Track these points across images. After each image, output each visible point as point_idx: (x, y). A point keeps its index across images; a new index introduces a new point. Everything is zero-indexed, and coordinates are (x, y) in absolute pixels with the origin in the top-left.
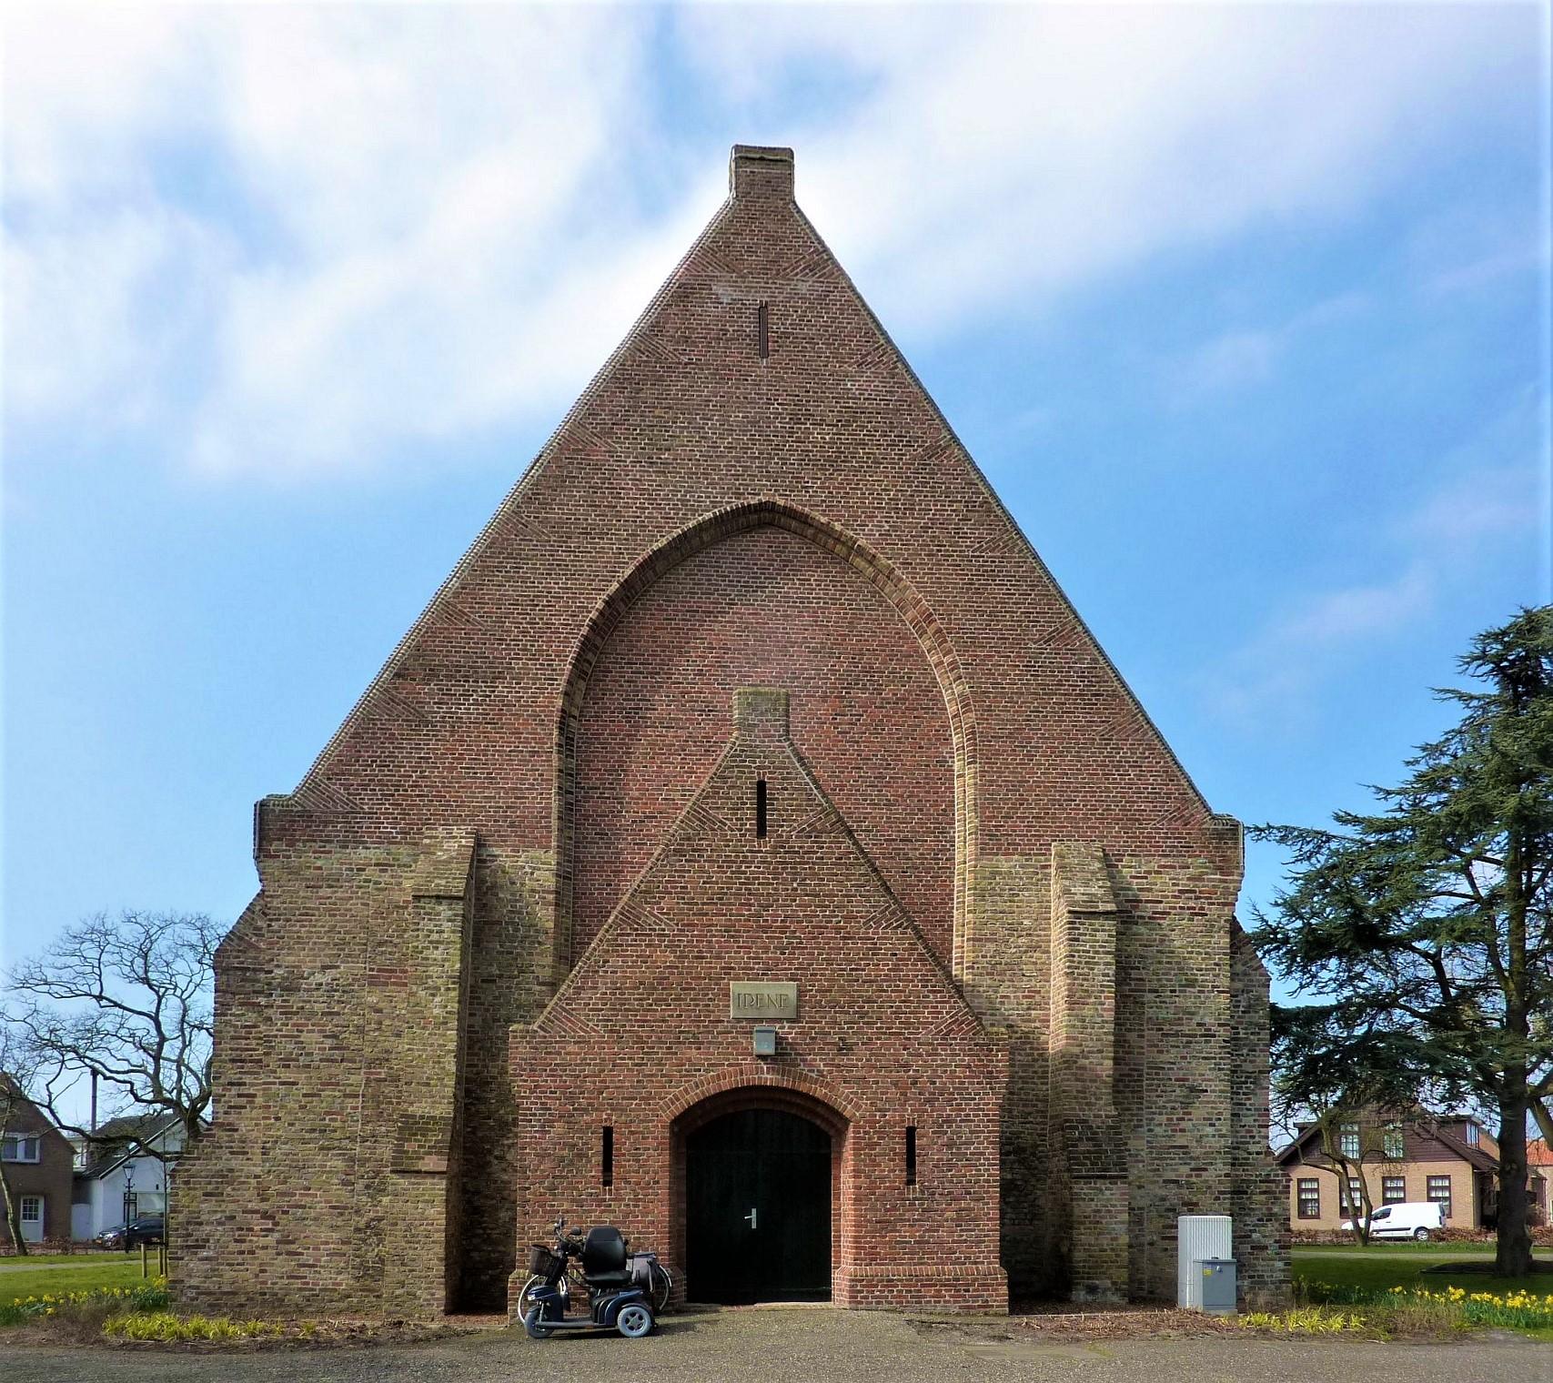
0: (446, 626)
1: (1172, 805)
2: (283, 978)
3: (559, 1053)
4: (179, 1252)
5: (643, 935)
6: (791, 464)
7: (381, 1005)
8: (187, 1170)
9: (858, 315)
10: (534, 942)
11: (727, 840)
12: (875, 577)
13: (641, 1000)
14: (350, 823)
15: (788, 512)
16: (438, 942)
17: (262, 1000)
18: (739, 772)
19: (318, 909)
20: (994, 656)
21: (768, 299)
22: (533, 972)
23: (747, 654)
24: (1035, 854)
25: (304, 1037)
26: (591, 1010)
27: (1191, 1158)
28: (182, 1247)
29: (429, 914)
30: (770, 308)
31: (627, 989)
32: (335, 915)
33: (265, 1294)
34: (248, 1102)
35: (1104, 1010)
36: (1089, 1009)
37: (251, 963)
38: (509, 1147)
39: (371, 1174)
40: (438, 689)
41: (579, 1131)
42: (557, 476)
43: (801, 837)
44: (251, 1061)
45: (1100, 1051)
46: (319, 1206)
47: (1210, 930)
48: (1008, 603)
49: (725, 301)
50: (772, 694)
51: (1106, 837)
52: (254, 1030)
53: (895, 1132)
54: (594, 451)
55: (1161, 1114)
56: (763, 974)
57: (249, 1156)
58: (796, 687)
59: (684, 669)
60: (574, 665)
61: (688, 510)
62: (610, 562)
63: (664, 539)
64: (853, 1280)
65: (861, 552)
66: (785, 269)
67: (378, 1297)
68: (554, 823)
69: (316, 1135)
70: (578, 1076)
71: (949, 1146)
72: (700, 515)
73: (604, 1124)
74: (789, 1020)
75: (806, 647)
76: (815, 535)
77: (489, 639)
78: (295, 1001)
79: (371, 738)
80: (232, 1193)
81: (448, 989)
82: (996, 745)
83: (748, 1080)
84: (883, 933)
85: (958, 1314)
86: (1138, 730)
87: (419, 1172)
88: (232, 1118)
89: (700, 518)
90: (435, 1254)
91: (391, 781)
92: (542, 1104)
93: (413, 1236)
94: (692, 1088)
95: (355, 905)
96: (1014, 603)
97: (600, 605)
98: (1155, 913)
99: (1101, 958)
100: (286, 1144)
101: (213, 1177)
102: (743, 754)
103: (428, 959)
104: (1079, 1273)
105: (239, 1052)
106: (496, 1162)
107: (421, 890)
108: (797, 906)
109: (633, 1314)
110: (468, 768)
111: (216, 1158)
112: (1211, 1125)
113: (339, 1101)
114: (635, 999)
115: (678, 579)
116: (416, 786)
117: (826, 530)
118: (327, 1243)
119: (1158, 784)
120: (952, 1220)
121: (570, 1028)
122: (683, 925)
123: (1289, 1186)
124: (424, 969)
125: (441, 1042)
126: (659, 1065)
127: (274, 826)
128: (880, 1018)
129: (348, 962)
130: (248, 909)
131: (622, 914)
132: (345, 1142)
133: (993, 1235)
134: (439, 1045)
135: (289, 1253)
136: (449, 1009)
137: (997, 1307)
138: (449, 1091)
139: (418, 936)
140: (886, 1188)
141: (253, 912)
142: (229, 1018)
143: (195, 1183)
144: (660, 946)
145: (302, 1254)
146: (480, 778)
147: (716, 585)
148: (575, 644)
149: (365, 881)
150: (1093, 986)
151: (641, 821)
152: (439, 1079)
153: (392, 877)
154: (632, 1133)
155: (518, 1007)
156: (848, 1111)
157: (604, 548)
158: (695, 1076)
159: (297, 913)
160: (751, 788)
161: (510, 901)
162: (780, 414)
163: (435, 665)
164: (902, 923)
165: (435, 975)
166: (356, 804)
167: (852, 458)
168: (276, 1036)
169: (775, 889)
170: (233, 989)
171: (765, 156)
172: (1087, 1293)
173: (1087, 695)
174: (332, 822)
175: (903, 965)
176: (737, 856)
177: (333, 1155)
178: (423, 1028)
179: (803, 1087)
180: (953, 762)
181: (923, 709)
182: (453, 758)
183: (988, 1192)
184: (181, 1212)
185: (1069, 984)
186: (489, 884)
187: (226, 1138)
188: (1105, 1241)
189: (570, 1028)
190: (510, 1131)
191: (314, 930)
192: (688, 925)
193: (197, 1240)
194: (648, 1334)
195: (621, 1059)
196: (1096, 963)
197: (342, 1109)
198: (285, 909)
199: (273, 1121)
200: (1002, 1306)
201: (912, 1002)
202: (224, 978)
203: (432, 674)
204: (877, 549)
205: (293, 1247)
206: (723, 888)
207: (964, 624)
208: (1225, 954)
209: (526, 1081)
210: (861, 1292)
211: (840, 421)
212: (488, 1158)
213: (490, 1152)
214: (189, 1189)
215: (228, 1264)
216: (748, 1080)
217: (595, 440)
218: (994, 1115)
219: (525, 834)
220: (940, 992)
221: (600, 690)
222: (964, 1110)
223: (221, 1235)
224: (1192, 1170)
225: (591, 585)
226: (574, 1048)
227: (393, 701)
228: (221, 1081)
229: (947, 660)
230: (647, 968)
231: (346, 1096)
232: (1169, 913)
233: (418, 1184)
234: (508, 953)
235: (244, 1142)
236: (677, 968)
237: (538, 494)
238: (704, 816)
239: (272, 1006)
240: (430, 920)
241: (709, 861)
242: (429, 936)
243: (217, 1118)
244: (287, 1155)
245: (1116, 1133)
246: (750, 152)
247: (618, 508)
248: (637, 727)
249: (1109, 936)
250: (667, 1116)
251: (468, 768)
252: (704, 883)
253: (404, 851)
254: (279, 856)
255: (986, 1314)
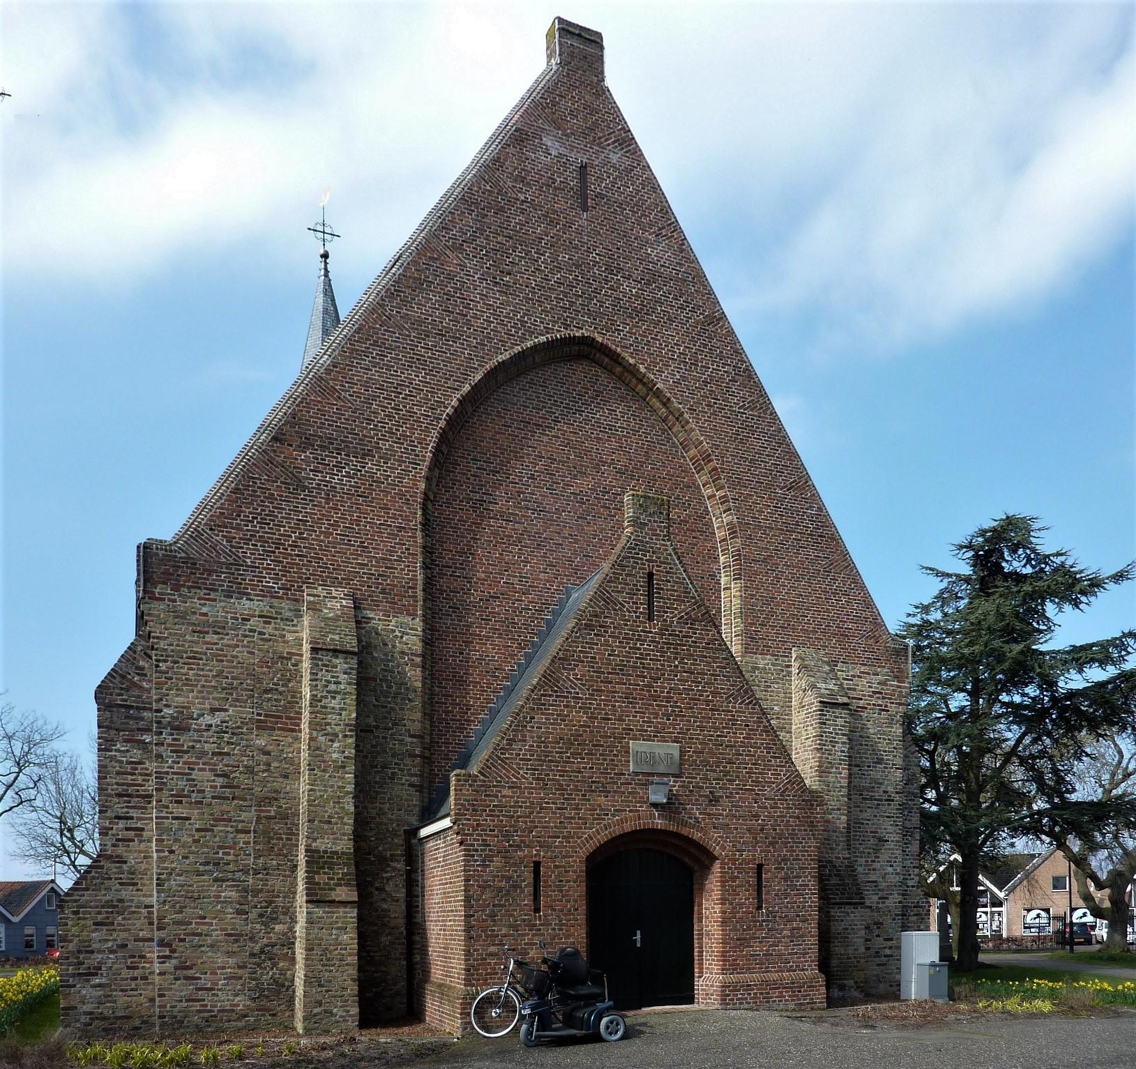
0: (319, 399)
1: (868, 627)
2: (172, 717)
3: (497, 796)
4: (71, 980)
5: (561, 696)
6: (606, 307)
7: (269, 748)
8: (76, 901)
9: (655, 192)
10: (404, 699)
11: (626, 620)
12: (667, 417)
13: (561, 753)
14: (233, 574)
15: (604, 349)
16: (336, 692)
17: (147, 738)
18: (634, 562)
19: (206, 654)
20: (753, 496)
21: (587, 161)
22: (405, 725)
23: (568, 466)
24: (782, 656)
25: (195, 774)
26: (521, 760)
27: (879, 890)
28: (73, 975)
29: (327, 666)
30: (588, 169)
31: (549, 742)
32: (222, 661)
33: (164, 1017)
34: (136, 835)
35: (841, 778)
36: (832, 777)
37: (134, 702)
38: (388, 879)
39: (264, 904)
40: (313, 458)
41: (515, 864)
42: (414, 278)
43: (680, 623)
44: (138, 796)
45: (839, 809)
46: (215, 933)
47: (890, 724)
48: (763, 454)
49: (553, 153)
50: (658, 499)
51: (827, 647)
52: (139, 766)
53: (749, 868)
54: (447, 262)
55: (861, 857)
56: (654, 736)
57: (139, 887)
58: (606, 500)
59: (520, 470)
60: (434, 454)
61: (526, 331)
62: (462, 365)
63: (507, 353)
64: (723, 986)
65: (658, 394)
66: (600, 138)
67: (274, 1015)
68: (420, 594)
69: (210, 867)
70: (513, 817)
71: (786, 879)
72: (536, 338)
73: (534, 859)
74: (674, 776)
75: (614, 468)
76: (622, 373)
77: (359, 418)
78: (185, 740)
79: (251, 496)
80: (123, 922)
81: (346, 736)
82: (756, 567)
83: (644, 823)
84: (739, 708)
85: (794, 1010)
86: (847, 567)
87: (333, 901)
88: (121, 850)
89: (536, 340)
90: (348, 975)
91: (272, 538)
92: (483, 840)
93: (328, 960)
94: (601, 829)
95: (241, 653)
96: (766, 455)
97: (455, 403)
98: (858, 707)
99: (839, 739)
100: (181, 875)
101: (103, 907)
102: (636, 547)
103: (326, 707)
104: (834, 975)
105: (125, 787)
106: (377, 893)
107: (318, 643)
108: (678, 680)
109: (611, 1022)
110: (343, 535)
111: (105, 889)
112: (891, 866)
113: (232, 836)
114: (557, 752)
115: (513, 392)
116: (296, 546)
117: (632, 371)
118: (224, 968)
119: (860, 610)
120: (788, 937)
121: (504, 774)
122: (593, 690)
123: (929, 911)
124: (324, 716)
125: (340, 784)
126: (576, 809)
127: (158, 570)
128: (738, 777)
129: (236, 706)
130: (129, 648)
131: (545, 677)
132: (238, 875)
133: (814, 949)
134: (339, 787)
135: (187, 978)
136: (346, 754)
137: (820, 1003)
138: (349, 829)
139: (317, 685)
140: (743, 912)
141: (135, 652)
142: (113, 753)
143: (84, 913)
144: (575, 707)
145: (200, 979)
146: (354, 546)
147: (544, 402)
148: (434, 435)
149: (251, 631)
150: (834, 759)
151: (486, 600)
152: (339, 818)
153: (276, 629)
154: (556, 867)
155: (394, 755)
156: (717, 851)
157: (457, 351)
158: (604, 819)
159: (185, 655)
160: (643, 578)
161: (382, 660)
162: (597, 262)
163: (310, 435)
164: (752, 701)
165: (333, 722)
166: (239, 557)
167: (653, 312)
168: (167, 773)
169: (662, 665)
170: (117, 726)
171: (583, 34)
172: (839, 990)
173: (815, 535)
174: (216, 571)
175: (753, 734)
176: (633, 635)
177: (227, 886)
178: (324, 771)
179: (684, 831)
180: (720, 577)
181: (699, 531)
182: (328, 524)
183: (810, 915)
184: (71, 941)
185: (819, 757)
186: (364, 643)
187: (114, 870)
188: (850, 951)
189: (504, 774)
190: (389, 866)
191: (201, 673)
192: (597, 690)
193: (89, 968)
194: (622, 1038)
195: (546, 803)
196: (837, 742)
197: (235, 843)
198: (172, 651)
199: (166, 854)
200: (823, 1003)
201: (760, 765)
202: (108, 714)
203: (307, 444)
204: (671, 393)
205: (191, 973)
206: (623, 661)
207: (733, 467)
208: (900, 741)
209: (469, 820)
210: (729, 995)
211: (643, 279)
212: (370, 889)
213: (371, 884)
214: (79, 919)
215: (122, 990)
216: (644, 823)
217: (448, 252)
218: (815, 855)
219: (395, 601)
220: (779, 758)
221: (451, 480)
222: (795, 851)
223: (113, 963)
224: (880, 898)
225: (447, 383)
226: (506, 792)
227: (272, 463)
228: (108, 814)
229: (719, 494)
230: (566, 725)
231: (238, 831)
232: (866, 708)
233: (333, 913)
234: (383, 707)
235: (133, 873)
236: (589, 727)
237: (400, 291)
238: (607, 597)
239: (163, 745)
240: (327, 671)
241: (612, 637)
242: (327, 687)
243: (105, 850)
244: (182, 886)
245: (852, 871)
246: (571, 26)
247: (469, 318)
248: (481, 516)
249: (845, 722)
250: (583, 853)
251: (343, 535)
252: (609, 655)
253: (285, 605)
254: (164, 599)
255: (812, 1009)
